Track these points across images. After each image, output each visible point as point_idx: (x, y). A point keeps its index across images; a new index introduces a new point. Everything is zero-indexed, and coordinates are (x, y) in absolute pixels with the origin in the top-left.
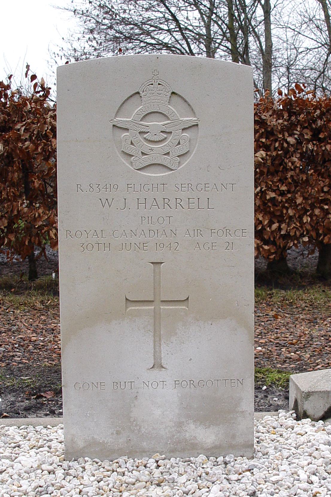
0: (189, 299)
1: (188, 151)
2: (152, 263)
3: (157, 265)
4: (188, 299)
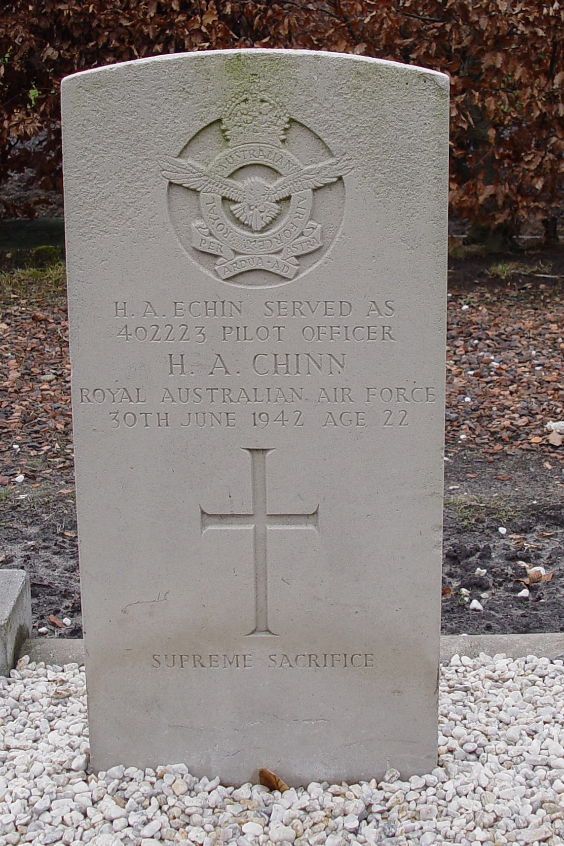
1: (321, 247)
3: (259, 456)
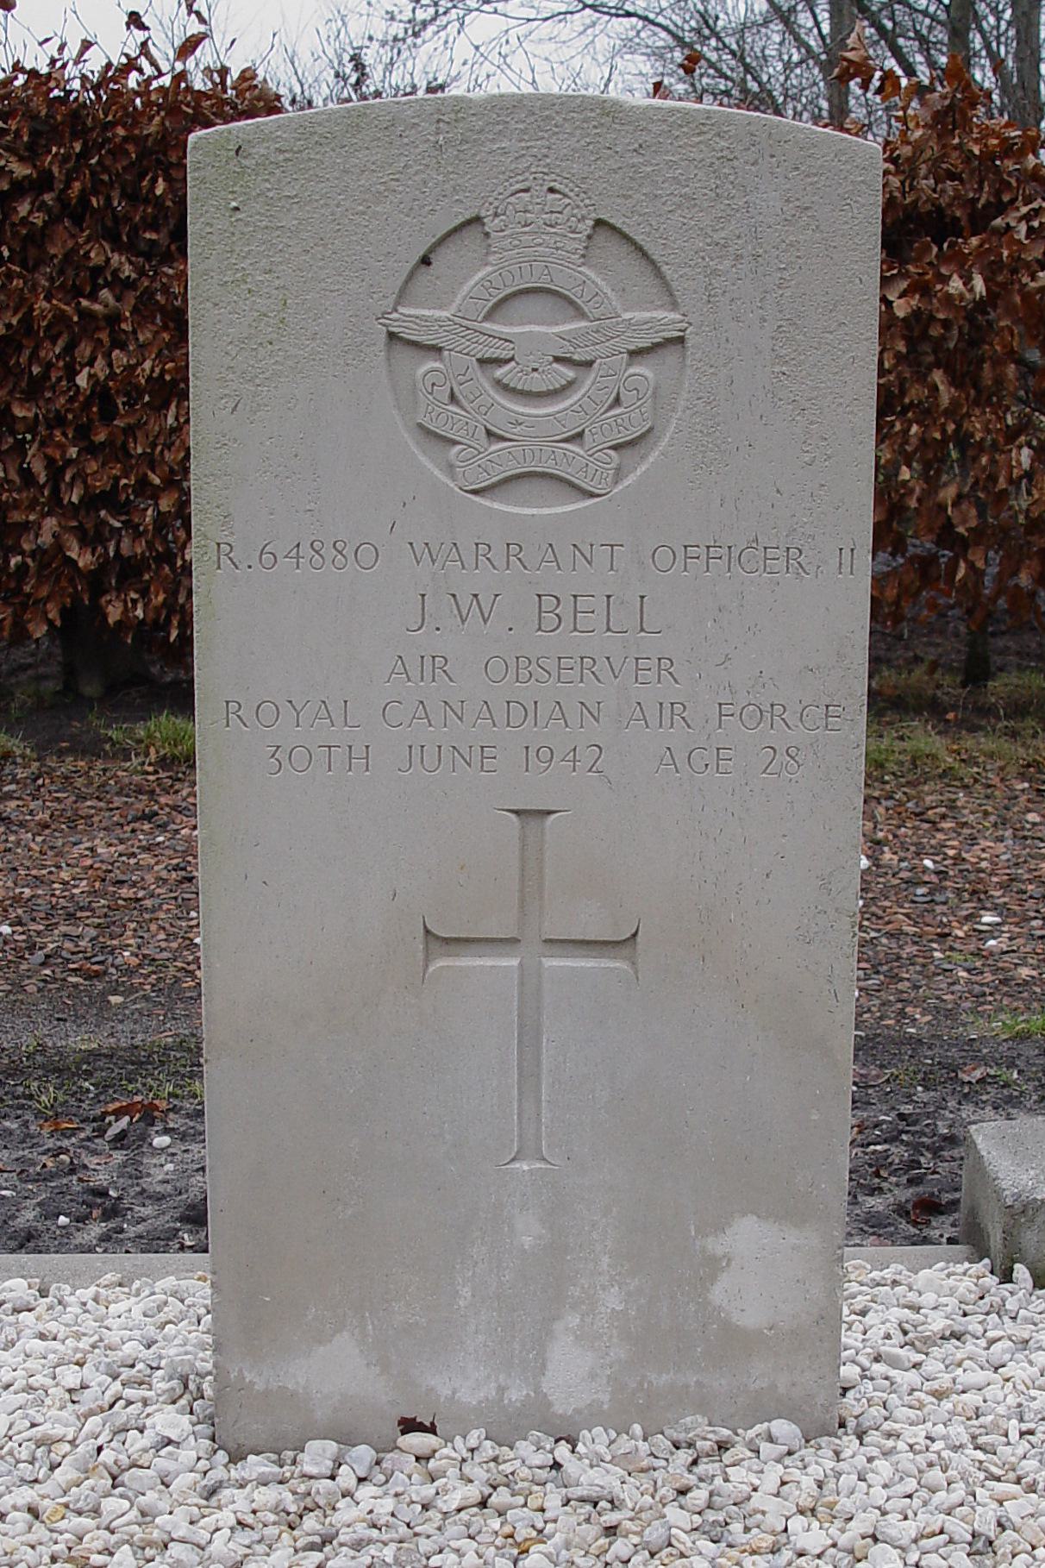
0: (639, 939)
2: (516, 812)
4: (635, 935)
